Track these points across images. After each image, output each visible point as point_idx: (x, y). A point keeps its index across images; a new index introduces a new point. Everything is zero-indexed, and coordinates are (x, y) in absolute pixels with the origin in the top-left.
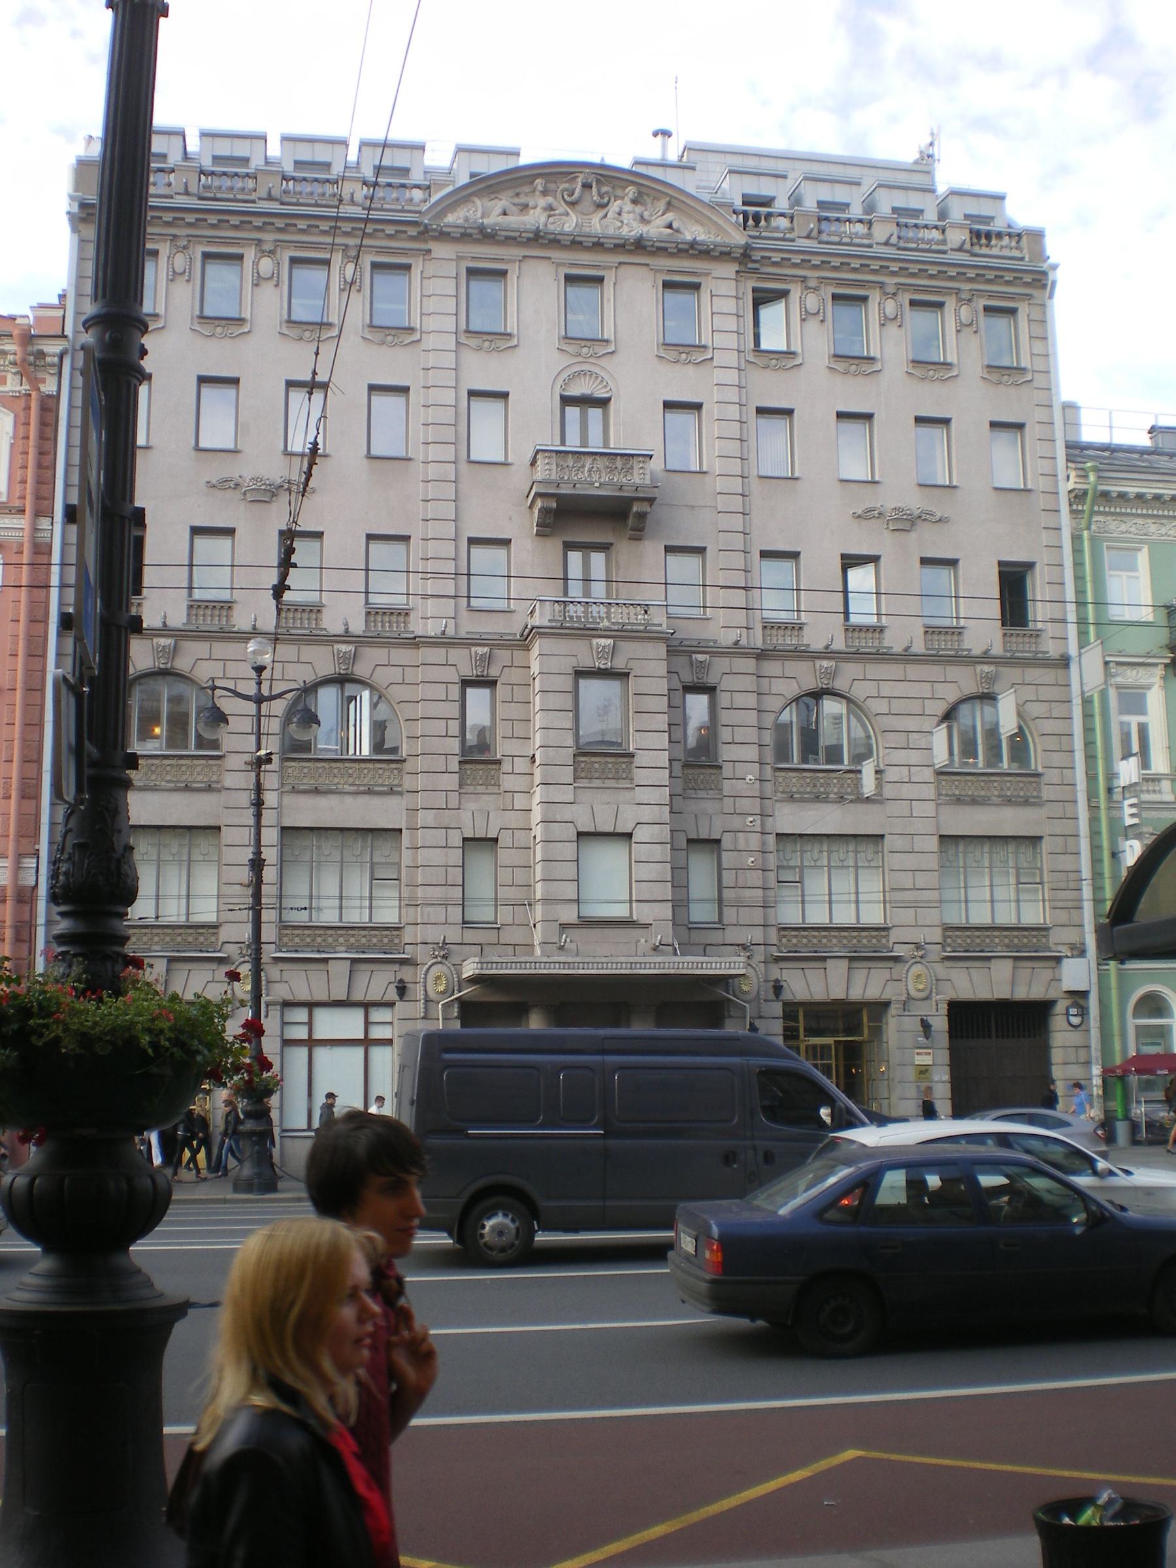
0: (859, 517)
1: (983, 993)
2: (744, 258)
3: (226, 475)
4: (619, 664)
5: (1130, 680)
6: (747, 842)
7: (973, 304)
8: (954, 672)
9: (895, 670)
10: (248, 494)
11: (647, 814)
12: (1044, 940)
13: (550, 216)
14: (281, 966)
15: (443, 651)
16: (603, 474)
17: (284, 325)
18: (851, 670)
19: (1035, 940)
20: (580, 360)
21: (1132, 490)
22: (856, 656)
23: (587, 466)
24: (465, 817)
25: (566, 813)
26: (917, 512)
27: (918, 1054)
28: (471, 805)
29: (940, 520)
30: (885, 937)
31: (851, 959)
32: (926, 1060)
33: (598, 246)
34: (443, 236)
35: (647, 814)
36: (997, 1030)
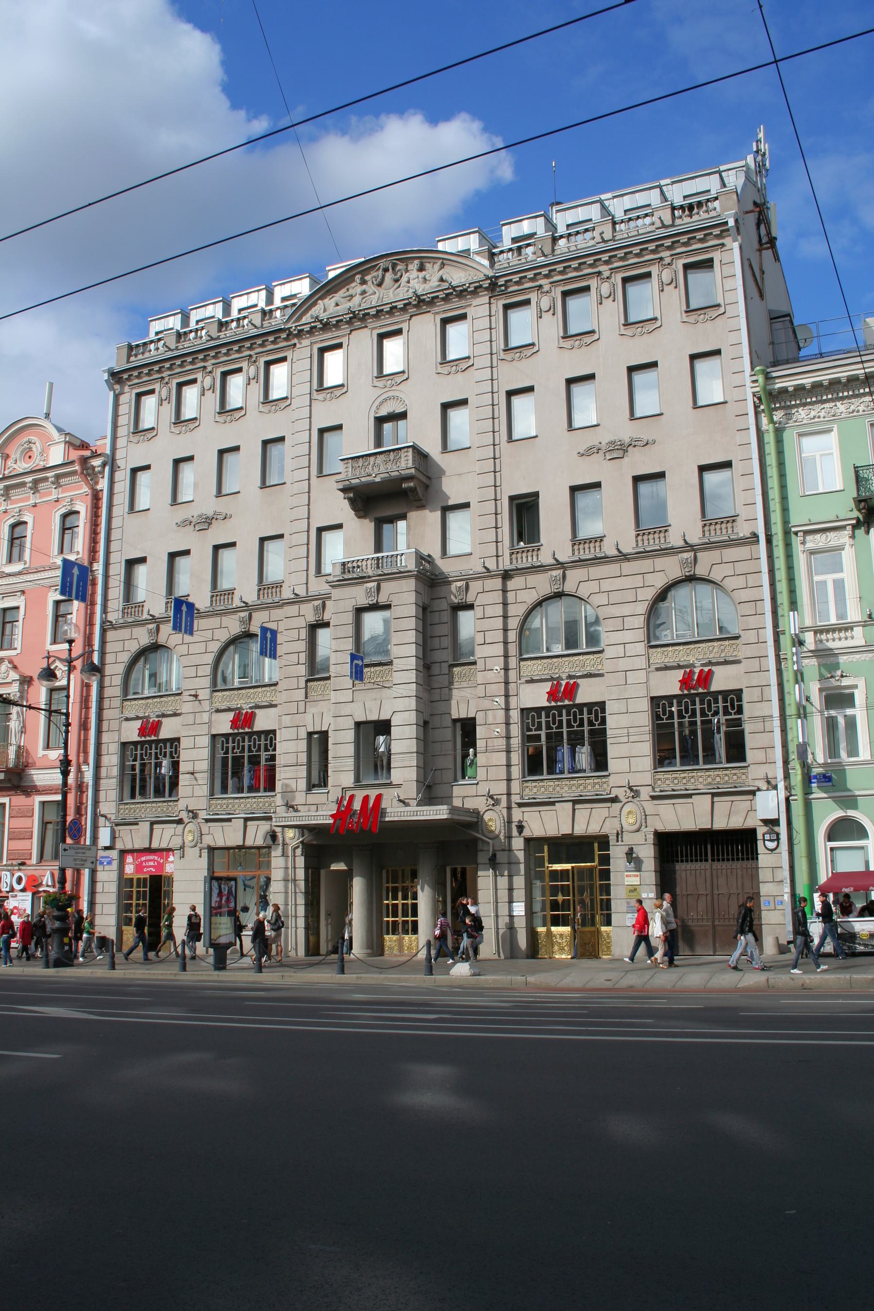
0: (583, 455)
1: (689, 825)
2: (493, 287)
3: (589, 445)
4: (383, 599)
5: (821, 544)
6: (494, 717)
7: (613, 280)
8: (661, 562)
9: (612, 569)
10: (607, 454)
11: (401, 704)
12: (744, 777)
13: (363, 298)
14: (210, 824)
15: (296, 607)
16: (381, 467)
17: (622, 327)
18: (574, 576)
19: (735, 777)
20: (386, 389)
21: (807, 381)
22: (709, 546)
23: (372, 463)
24: (308, 718)
25: (346, 709)
26: (627, 441)
27: (627, 876)
28: (312, 709)
29: (647, 444)
30: (744, 774)
31: (714, 795)
32: (635, 881)
33: (393, 310)
34: (300, 334)
35: (401, 704)
36: (713, 855)
